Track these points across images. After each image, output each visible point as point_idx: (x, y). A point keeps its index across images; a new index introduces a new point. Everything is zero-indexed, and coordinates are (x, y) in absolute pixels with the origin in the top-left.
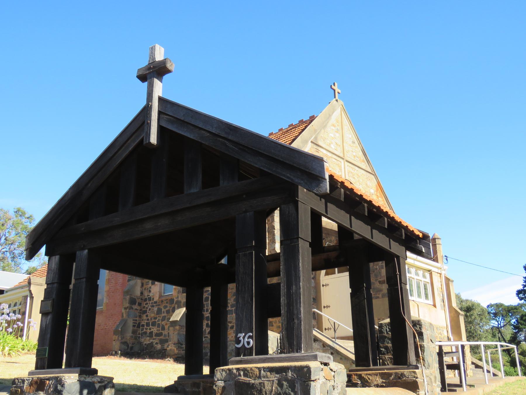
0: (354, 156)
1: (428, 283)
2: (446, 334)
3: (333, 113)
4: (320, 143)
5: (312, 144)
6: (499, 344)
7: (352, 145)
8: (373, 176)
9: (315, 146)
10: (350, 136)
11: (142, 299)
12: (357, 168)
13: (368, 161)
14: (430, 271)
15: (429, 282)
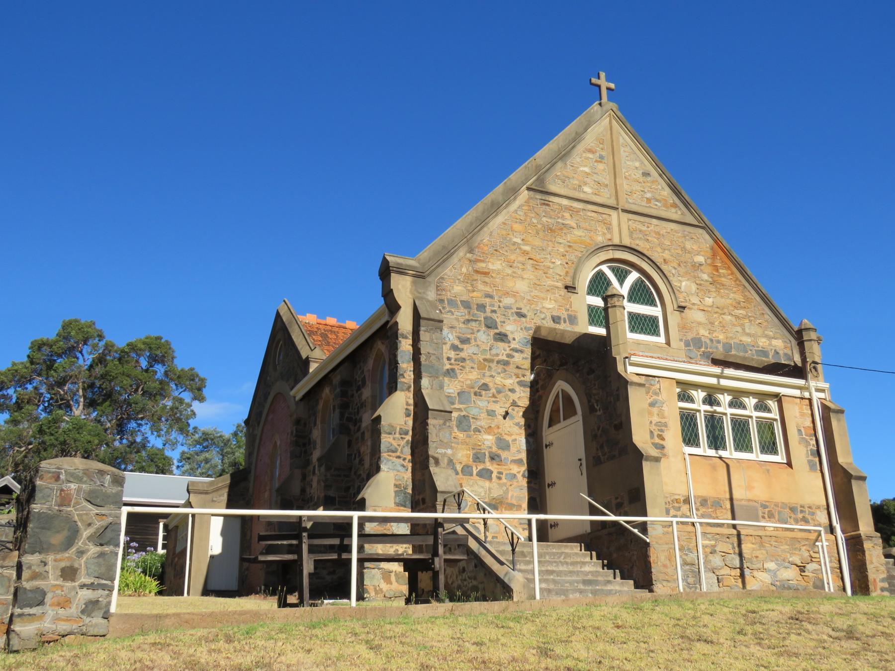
0: (649, 200)
1: (776, 420)
2: (824, 519)
3: (586, 129)
4: (553, 188)
5: (531, 193)
6: (675, 520)
7: (642, 179)
8: (701, 231)
9: (539, 196)
10: (637, 164)
11: (303, 500)
12: (654, 221)
13: (686, 204)
14: (778, 397)
15: (778, 417)
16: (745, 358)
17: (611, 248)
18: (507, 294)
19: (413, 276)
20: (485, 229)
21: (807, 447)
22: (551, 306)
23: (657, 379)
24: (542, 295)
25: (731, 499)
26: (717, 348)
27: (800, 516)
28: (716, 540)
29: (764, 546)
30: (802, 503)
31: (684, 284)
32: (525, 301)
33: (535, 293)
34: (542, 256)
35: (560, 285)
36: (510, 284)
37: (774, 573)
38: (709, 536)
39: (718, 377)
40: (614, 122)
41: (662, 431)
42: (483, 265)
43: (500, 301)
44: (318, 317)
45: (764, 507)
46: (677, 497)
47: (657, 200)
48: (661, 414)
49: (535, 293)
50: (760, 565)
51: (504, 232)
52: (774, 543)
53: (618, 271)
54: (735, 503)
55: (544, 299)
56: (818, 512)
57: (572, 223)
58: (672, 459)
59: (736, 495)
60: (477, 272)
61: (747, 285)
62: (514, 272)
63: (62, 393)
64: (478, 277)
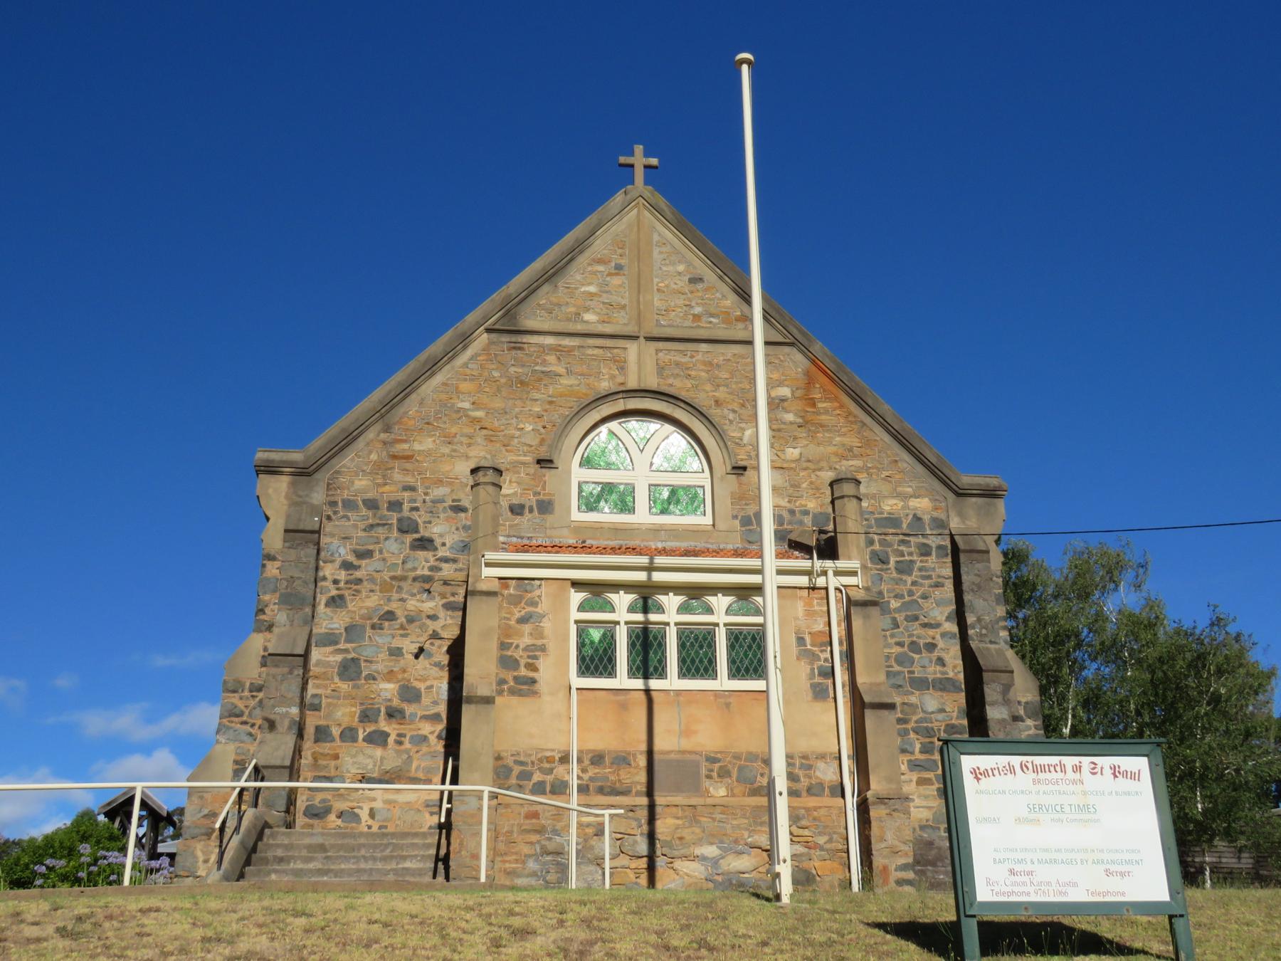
5: (493, 336)
12: (704, 347)
18: (440, 482)
19: (292, 474)
20: (413, 396)
23: (537, 582)
25: (650, 753)
26: (801, 523)
29: (698, 822)
34: (504, 421)
35: (529, 459)
36: (446, 467)
37: (715, 862)
41: (536, 658)
42: (406, 446)
43: (426, 494)
45: (713, 760)
46: (548, 754)
47: (712, 315)
50: (683, 852)
51: (443, 396)
54: (657, 757)
56: (821, 765)
57: (561, 370)
58: (546, 698)
59: (660, 744)
60: (394, 457)
61: (868, 420)
62: (455, 451)
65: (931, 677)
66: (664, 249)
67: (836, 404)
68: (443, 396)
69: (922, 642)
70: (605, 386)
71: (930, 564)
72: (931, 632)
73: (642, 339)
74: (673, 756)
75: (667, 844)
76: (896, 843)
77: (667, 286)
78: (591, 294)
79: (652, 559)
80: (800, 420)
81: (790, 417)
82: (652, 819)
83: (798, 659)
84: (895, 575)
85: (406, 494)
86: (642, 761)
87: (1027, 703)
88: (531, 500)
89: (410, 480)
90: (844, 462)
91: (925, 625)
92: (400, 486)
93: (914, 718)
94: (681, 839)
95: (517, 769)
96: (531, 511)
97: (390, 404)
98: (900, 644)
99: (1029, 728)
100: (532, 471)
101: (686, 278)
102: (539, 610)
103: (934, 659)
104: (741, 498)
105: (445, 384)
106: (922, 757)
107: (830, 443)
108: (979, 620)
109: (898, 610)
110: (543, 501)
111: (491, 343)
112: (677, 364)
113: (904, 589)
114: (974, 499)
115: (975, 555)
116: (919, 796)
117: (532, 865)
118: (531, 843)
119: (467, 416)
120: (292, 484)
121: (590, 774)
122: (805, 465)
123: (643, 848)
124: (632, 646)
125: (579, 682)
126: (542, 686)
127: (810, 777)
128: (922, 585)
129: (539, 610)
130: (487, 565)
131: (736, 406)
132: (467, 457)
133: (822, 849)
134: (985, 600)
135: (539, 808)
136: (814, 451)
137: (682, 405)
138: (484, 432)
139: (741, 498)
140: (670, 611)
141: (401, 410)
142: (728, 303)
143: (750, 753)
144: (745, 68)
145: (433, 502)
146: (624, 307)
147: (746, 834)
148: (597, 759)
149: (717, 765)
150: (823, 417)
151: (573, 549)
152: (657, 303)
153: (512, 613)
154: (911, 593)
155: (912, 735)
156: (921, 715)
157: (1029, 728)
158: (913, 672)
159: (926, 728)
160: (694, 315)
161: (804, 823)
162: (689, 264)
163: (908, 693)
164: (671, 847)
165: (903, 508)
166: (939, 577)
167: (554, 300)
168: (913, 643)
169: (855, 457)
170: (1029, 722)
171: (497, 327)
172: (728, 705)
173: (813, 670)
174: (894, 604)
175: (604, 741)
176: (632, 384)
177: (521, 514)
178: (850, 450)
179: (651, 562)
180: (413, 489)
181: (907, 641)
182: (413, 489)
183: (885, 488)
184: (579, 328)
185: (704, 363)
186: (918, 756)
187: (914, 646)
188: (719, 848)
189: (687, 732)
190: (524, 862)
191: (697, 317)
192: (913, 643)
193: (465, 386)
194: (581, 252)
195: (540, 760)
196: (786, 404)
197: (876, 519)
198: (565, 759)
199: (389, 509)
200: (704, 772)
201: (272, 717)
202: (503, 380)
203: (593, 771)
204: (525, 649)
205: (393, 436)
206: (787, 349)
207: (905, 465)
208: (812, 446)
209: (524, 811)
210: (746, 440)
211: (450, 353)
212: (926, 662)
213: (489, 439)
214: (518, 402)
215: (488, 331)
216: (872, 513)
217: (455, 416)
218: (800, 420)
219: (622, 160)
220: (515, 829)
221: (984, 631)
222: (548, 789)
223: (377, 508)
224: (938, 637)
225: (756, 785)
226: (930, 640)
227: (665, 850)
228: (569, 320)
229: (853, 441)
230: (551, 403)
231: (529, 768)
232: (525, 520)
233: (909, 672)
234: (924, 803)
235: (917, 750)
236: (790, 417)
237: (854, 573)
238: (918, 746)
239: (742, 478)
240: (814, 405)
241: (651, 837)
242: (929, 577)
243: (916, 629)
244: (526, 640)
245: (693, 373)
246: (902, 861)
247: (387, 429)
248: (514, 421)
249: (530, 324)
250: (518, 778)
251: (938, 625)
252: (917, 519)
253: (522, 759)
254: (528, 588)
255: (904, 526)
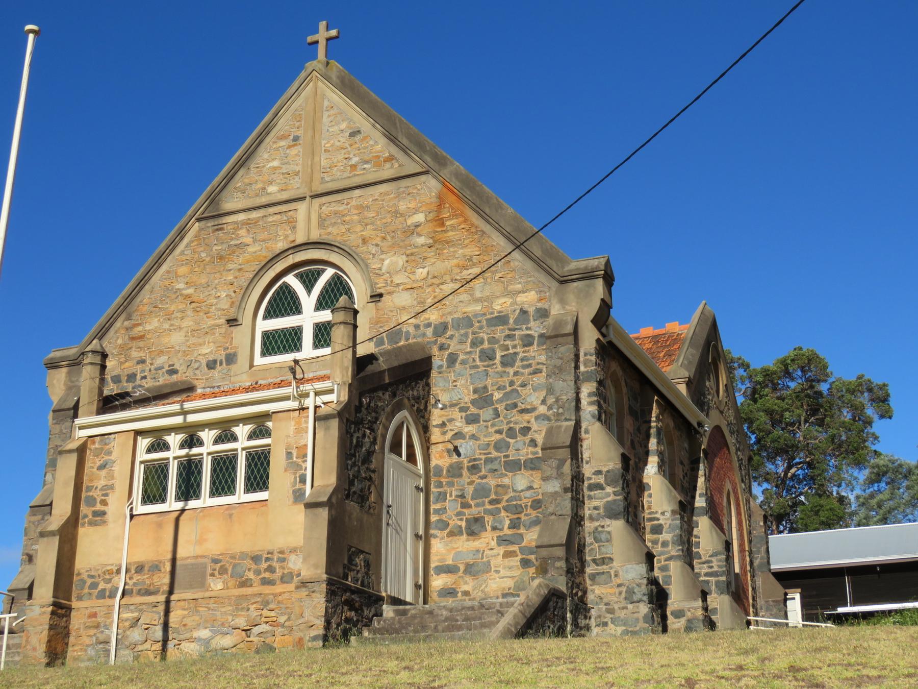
5: (203, 223)
12: (357, 192)
16: (161, 386)
17: (290, 252)
18: (161, 353)
19: (68, 366)
20: (147, 287)
21: (295, 473)
22: (207, 351)
23: (113, 436)
24: (201, 340)
25: (174, 560)
26: (424, 335)
27: (264, 565)
28: (141, 611)
29: (197, 611)
30: (269, 547)
31: (387, 262)
32: (180, 354)
33: (192, 340)
34: (207, 293)
35: (223, 321)
36: (165, 340)
37: (207, 642)
38: (132, 607)
39: (184, 413)
40: (320, 83)
41: (107, 495)
42: (140, 328)
43: (151, 364)
44: (655, 329)
45: (215, 561)
46: (109, 568)
47: (366, 162)
48: (111, 476)
49: (192, 340)
50: (188, 635)
51: (167, 282)
52: (212, 606)
53: (307, 276)
54: (178, 563)
55: (200, 345)
56: (293, 557)
57: (248, 240)
58: (111, 525)
59: (181, 553)
60: (133, 339)
61: (487, 228)
62: (172, 325)
63: (844, 438)
64: (134, 344)
65: (523, 459)
66: (332, 112)
67: (461, 219)
68: (167, 282)
69: (517, 427)
70: (281, 245)
71: (532, 354)
72: (527, 417)
73: (308, 198)
74: (189, 561)
75: (177, 631)
76: (312, 619)
77: (332, 145)
78: (275, 168)
79: (182, 405)
80: (431, 241)
81: (421, 240)
82: (167, 612)
83: (286, 470)
84: (500, 368)
85: (139, 367)
86: (168, 567)
87: (608, 471)
88: (221, 355)
89: (142, 354)
90: (465, 272)
91: (523, 411)
92: (135, 361)
93: (506, 498)
94: (184, 625)
95: (89, 581)
96: (221, 364)
97: (131, 298)
98: (499, 432)
99: (608, 495)
100: (223, 330)
101: (347, 134)
102: (113, 458)
103: (527, 441)
104: (377, 323)
105: (168, 272)
106: (509, 532)
107: (454, 257)
108: (557, 400)
109: (500, 401)
110: (230, 354)
111: (201, 229)
112: (336, 213)
113: (505, 381)
114: (575, 284)
115: (560, 340)
116: (504, 568)
117: (91, 652)
118: (91, 636)
119: (182, 295)
120: (69, 373)
121: (134, 580)
122: (430, 281)
123: (159, 634)
124: (180, 475)
125: (140, 509)
126: (109, 517)
127: (284, 568)
128: (523, 374)
129: (113, 458)
130: (80, 428)
131: (378, 241)
132: (180, 328)
133: (283, 626)
134: (564, 381)
135: (97, 609)
136: (440, 266)
137: (336, 249)
138: (193, 305)
139: (377, 323)
140: (209, 446)
141: (138, 300)
142: (378, 147)
143: (242, 553)
144: (31, 37)
145: (156, 369)
146: (297, 173)
147: (230, 618)
148: (140, 569)
149: (219, 565)
150: (450, 234)
151: (247, 390)
152: (324, 163)
153: (94, 463)
154: (512, 383)
155: (503, 514)
156: (512, 494)
157: (608, 495)
158: (507, 456)
159: (516, 506)
160: (351, 166)
161: (271, 606)
162: (350, 120)
163: (503, 476)
164: (178, 633)
165: (512, 304)
166: (538, 364)
167: (246, 181)
168: (510, 429)
169: (474, 265)
170: (609, 489)
171: (205, 215)
172: (231, 515)
173: (295, 478)
174: (497, 395)
175: (144, 555)
176: (300, 239)
177: (213, 368)
178: (470, 260)
179: (182, 408)
180: (143, 362)
181: (505, 428)
182: (143, 362)
183: (498, 288)
184: (264, 200)
185: (357, 207)
186: (507, 531)
187: (511, 433)
188: (211, 630)
189: (201, 541)
190: (86, 651)
191: (354, 167)
192: (510, 429)
193: (183, 270)
194: (268, 133)
195: (104, 573)
196: (419, 229)
197: (487, 320)
198: (118, 571)
199: (128, 381)
200: (209, 571)
201: (31, 552)
202: (208, 259)
203: (136, 577)
204: (101, 490)
205: (133, 322)
206: (423, 178)
207: (517, 263)
208: (439, 263)
209: (87, 612)
210: (384, 270)
211: (172, 247)
212: (520, 445)
213: (195, 311)
214: (218, 275)
215: (198, 220)
216: (485, 314)
217: (174, 296)
218: (431, 241)
219: (310, 39)
220: (82, 626)
221: (561, 410)
222: (107, 594)
223: (120, 381)
224: (533, 420)
225: (244, 579)
226: (525, 424)
227: (175, 635)
228: (257, 195)
229: (472, 251)
230: (240, 270)
231: (96, 580)
232: (216, 373)
233: (505, 456)
234: (509, 574)
235: (506, 526)
236: (421, 240)
237: (331, 391)
238: (507, 522)
239: (379, 304)
240: (443, 224)
241: (166, 626)
242: (530, 366)
243: (514, 416)
244: (102, 483)
245: (347, 218)
246: (313, 633)
247: (129, 318)
248: (213, 292)
249: (228, 206)
250: (90, 588)
251: (534, 409)
252: (524, 312)
253: (93, 573)
254: (107, 441)
255: (511, 321)
